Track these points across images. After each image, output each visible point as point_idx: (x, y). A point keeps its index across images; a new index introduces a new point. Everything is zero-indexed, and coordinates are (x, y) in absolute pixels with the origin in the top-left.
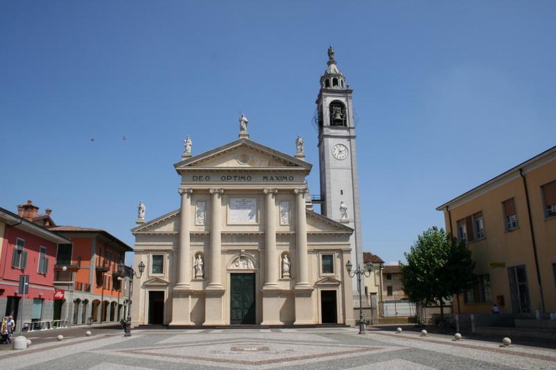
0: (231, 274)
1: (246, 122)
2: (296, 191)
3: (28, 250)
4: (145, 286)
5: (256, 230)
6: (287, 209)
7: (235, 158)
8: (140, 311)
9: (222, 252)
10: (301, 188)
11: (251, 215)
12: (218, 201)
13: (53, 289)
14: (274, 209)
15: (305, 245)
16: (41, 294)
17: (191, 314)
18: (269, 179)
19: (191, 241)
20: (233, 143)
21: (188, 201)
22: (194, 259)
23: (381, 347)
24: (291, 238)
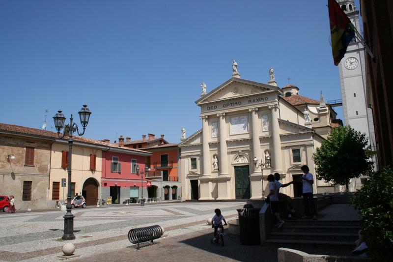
0: (235, 167)
1: (236, 66)
2: (270, 107)
3: (120, 162)
4: (188, 177)
5: (247, 136)
6: (267, 120)
7: (230, 91)
8: (187, 193)
9: (281, 148)
10: (221, 113)
11: (244, 127)
12: (223, 121)
13: (146, 181)
14: (257, 120)
15: (278, 143)
16: (135, 184)
17: (212, 193)
18: (252, 101)
19: (227, 146)
20: (227, 82)
21: (206, 123)
22: (264, 154)
23: (29, 223)
24: (268, 140)
